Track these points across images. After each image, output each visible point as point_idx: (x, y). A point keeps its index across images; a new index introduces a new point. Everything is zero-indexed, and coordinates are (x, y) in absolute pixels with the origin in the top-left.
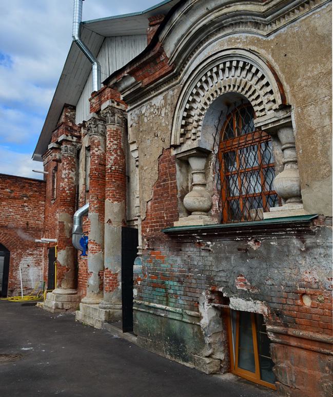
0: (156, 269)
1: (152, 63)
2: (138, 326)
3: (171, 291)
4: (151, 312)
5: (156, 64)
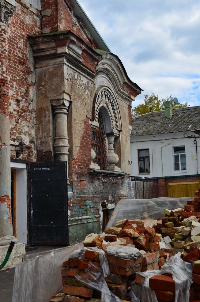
0: (81, 194)
1: (92, 59)
2: (71, 237)
3: (88, 207)
4: (80, 223)
5: (92, 61)
